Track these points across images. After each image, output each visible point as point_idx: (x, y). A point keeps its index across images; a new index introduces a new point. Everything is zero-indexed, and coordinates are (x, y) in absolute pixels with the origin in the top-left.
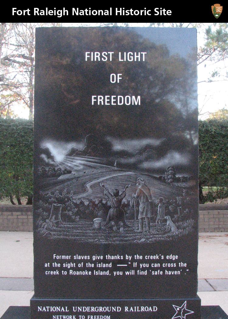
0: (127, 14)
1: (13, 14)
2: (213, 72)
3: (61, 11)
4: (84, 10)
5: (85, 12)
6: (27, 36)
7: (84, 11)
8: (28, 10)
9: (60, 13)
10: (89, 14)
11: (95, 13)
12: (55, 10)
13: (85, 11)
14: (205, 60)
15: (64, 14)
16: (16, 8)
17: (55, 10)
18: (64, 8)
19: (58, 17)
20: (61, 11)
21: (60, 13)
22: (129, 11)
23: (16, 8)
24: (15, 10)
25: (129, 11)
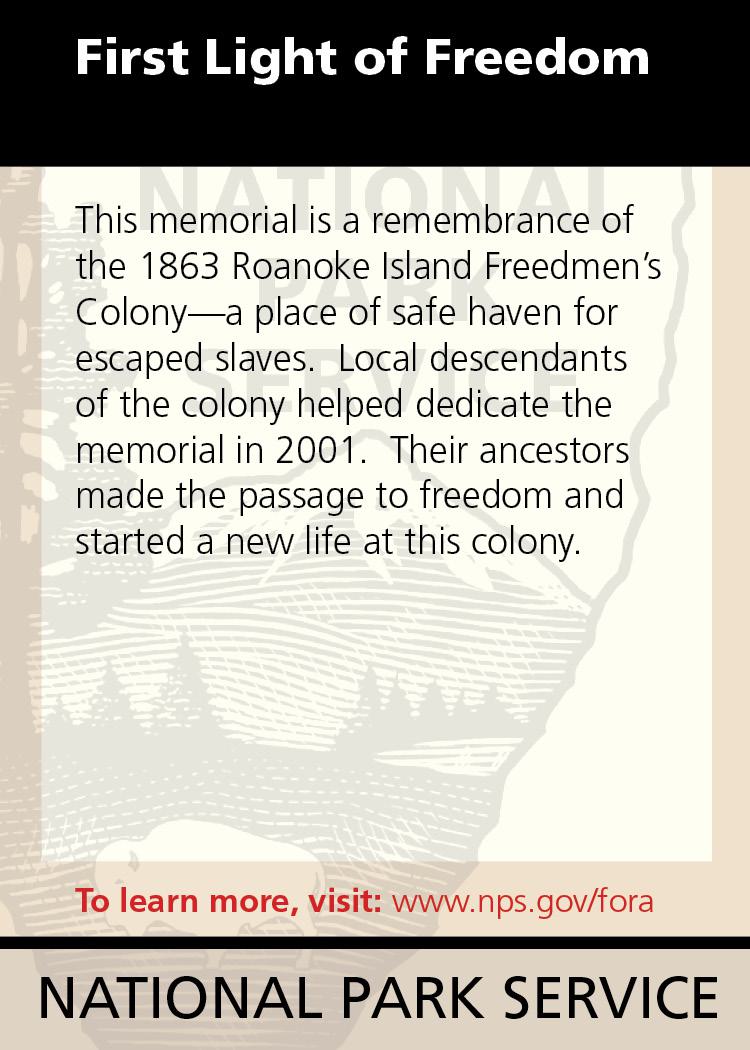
0: (153, 67)
1: (83, 69)
2: (378, 897)
3: (275, 54)
4: (314, 46)
5: (317, 60)
6: (166, 708)
7: (314, 53)
8: (178, 51)
9: (265, 61)
10: (234, 69)
11: (584, 61)
12: (240, 46)
13: (389, 52)
14: (36, 531)
15: (290, 70)
16: (446, 42)
17: (240, 46)
18: (289, 42)
19: (258, 81)
20: (275, 54)
21: (265, 61)
22: (160, 52)
23: (446, 42)
24: (440, 50)
25: (160, 52)
